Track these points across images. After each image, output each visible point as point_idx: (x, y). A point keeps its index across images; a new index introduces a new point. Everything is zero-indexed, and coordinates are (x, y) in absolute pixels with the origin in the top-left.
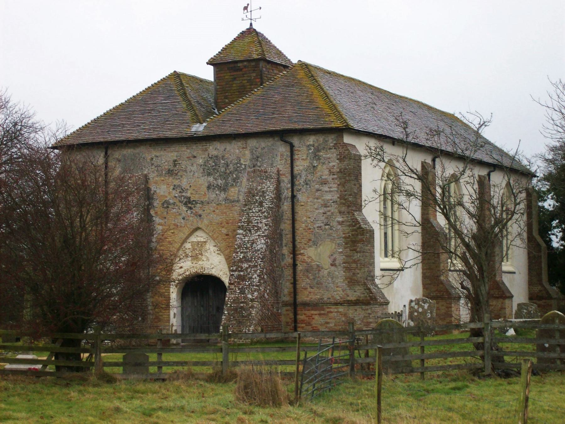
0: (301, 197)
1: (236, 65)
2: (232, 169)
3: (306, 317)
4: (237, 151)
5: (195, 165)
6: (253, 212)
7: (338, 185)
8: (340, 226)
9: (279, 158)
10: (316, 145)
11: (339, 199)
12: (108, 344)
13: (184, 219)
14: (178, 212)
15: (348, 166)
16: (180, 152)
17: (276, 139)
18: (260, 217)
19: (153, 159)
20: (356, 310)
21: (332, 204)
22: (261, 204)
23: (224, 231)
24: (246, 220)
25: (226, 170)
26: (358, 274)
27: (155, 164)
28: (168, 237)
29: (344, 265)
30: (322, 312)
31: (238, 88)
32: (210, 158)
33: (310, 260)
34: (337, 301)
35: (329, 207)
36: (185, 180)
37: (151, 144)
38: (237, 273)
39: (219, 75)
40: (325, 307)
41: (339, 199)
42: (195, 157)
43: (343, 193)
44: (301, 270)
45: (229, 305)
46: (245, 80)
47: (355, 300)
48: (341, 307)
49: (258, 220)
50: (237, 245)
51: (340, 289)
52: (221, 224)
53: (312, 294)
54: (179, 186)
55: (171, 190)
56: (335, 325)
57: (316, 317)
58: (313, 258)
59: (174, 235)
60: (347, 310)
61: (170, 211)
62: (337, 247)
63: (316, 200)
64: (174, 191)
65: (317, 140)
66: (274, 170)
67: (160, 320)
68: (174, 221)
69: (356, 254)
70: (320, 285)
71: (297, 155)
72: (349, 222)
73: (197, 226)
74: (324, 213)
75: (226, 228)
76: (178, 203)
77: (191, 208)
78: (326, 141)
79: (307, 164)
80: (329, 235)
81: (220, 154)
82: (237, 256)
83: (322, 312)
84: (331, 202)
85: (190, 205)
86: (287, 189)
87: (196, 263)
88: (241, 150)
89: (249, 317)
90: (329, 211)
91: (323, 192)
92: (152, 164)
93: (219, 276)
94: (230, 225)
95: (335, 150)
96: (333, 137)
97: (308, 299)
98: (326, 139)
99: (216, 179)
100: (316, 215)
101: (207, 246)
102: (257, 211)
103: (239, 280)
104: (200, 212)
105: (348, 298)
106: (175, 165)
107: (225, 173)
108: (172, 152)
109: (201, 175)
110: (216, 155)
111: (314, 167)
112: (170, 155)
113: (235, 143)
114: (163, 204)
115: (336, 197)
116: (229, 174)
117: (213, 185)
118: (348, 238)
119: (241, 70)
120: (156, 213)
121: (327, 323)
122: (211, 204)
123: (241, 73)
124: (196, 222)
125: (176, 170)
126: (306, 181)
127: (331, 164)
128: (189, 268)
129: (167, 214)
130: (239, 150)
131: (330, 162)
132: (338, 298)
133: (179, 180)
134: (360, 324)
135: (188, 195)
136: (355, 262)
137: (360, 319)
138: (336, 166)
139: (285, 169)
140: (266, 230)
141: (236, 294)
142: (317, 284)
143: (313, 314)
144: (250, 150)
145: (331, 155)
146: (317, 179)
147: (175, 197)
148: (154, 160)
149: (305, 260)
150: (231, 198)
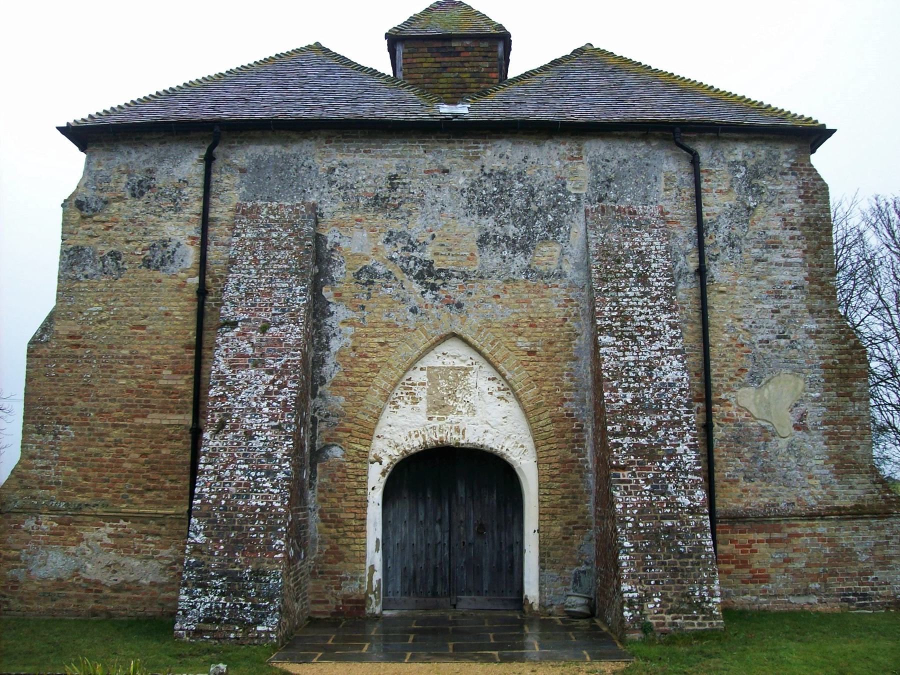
0: (717, 272)
1: (447, 44)
2: (544, 203)
3: (736, 547)
4: (557, 163)
5: (446, 190)
6: (627, 297)
7: (805, 252)
8: (812, 341)
9: (662, 185)
10: (751, 163)
11: (808, 282)
12: (268, 637)
13: (414, 311)
14: (398, 295)
15: (823, 212)
16: (407, 159)
17: (654, 144)
18: (650, 307)
19: (334, 170)
20: (857, 530)
21: (793, 291)
22: (643, 279)
23: (523, 343)
24: (615, 314)
25: (528, 203)
26: (858, 448)
27: (341, 182)
28: (370, 355)
29: (826, 427)
30: (776, 535)
31: (450, 85)
32: (485, 174)
33: (743, 416)
34: (811, 509)
35: (785, 297)
36: (418, 222)
37: (330, 137)
38: (627, 439)
39: (409, 61)
40: (782, 523)
41: (808, 282)
42: (446, 171)
43: (817, 269)
44: (723, 439)
45: (630, 525)
46: (465, 72)
47: (852, 508)
48: (821, 522)
49: (648, 314)
50: (608, 371)
51: (818, 481)
52: (516, 327)
53: (750, 494)
54: (402, 235)
55: (380, 244)
56: (808, 565)
57: (762, 548)
58: (753, 410)
59: (386, 350)
60: (836, 530)
61: (377, 291)
62: (807, 388)
63: (754, 282)
64: (388, 248)
65: (754, 153)
66: (653, 209)
67: (341, 557)
68: (388, 316)
69: (851, 404)
70: (769, 474)
71: (706, 181)
72: (833, 332)
73: (448, 330)
74: (773, 311)
75: (529, 337)
76: (398, 275)
77: (434, 287)
78: (775, 157)
79: (731, 202)
80: (789, 360)
81: (512, 167)
82: (615, 397)
83: (776, 535)
84: (790, 286)
85: (431, 281)
86: (686, 254)
87: (439, 419)
88: (566, 162)
89: (699, 557)
90: (786, 307)
91: (771, 264)
92: (332, 183)
93: (504, 450)
94: (539, 329)
95: (794, 177)
96: (789, 150)
97: (741, 505)
98: (775, 153)
99: (502, 224)
100: (757, 315)
101: (472, 379)
102: (638, 294)
103: (639, 459)
104: (460, 297)
105: (837, 503)
106: (393, 188)
107: (527, 211)
108: (387, 157)
109: (462, 212)
110: (502, 169)
111: (749, 209)
112: (380, 163)
113: (553, 146)
114: (358, 275)
115: (800, 276)
116: (536, 213)
117: (495, 237)
118: (832, 368)
119: (458, 54)
120: (338, 295)
121: (788, 560)
122: (489, 281)
123: (457, 59)
124: (449, 321)
125: (394, 199)
126: (729, 238)
127: (787, 206)
128: (421, 429)
129: (368, 299)
130: (562, 162)
131: (783, 202)
132: (813, 502)
133: (403, 221)
134: (867, 560)
135: (428, 256)
136: (848, 421)
137: (866, 549)
138: (798, 210)
139: (682, 211)
140: (675, 337)
141: (643, 496)
142: (762, 470)
143: (753, 541)
144: (590, 163)
145: (786, 188)
146: (757, 236)
147: (392, 259)
148: (337, 172)
149: (733, 415)
150: (542, 268)
